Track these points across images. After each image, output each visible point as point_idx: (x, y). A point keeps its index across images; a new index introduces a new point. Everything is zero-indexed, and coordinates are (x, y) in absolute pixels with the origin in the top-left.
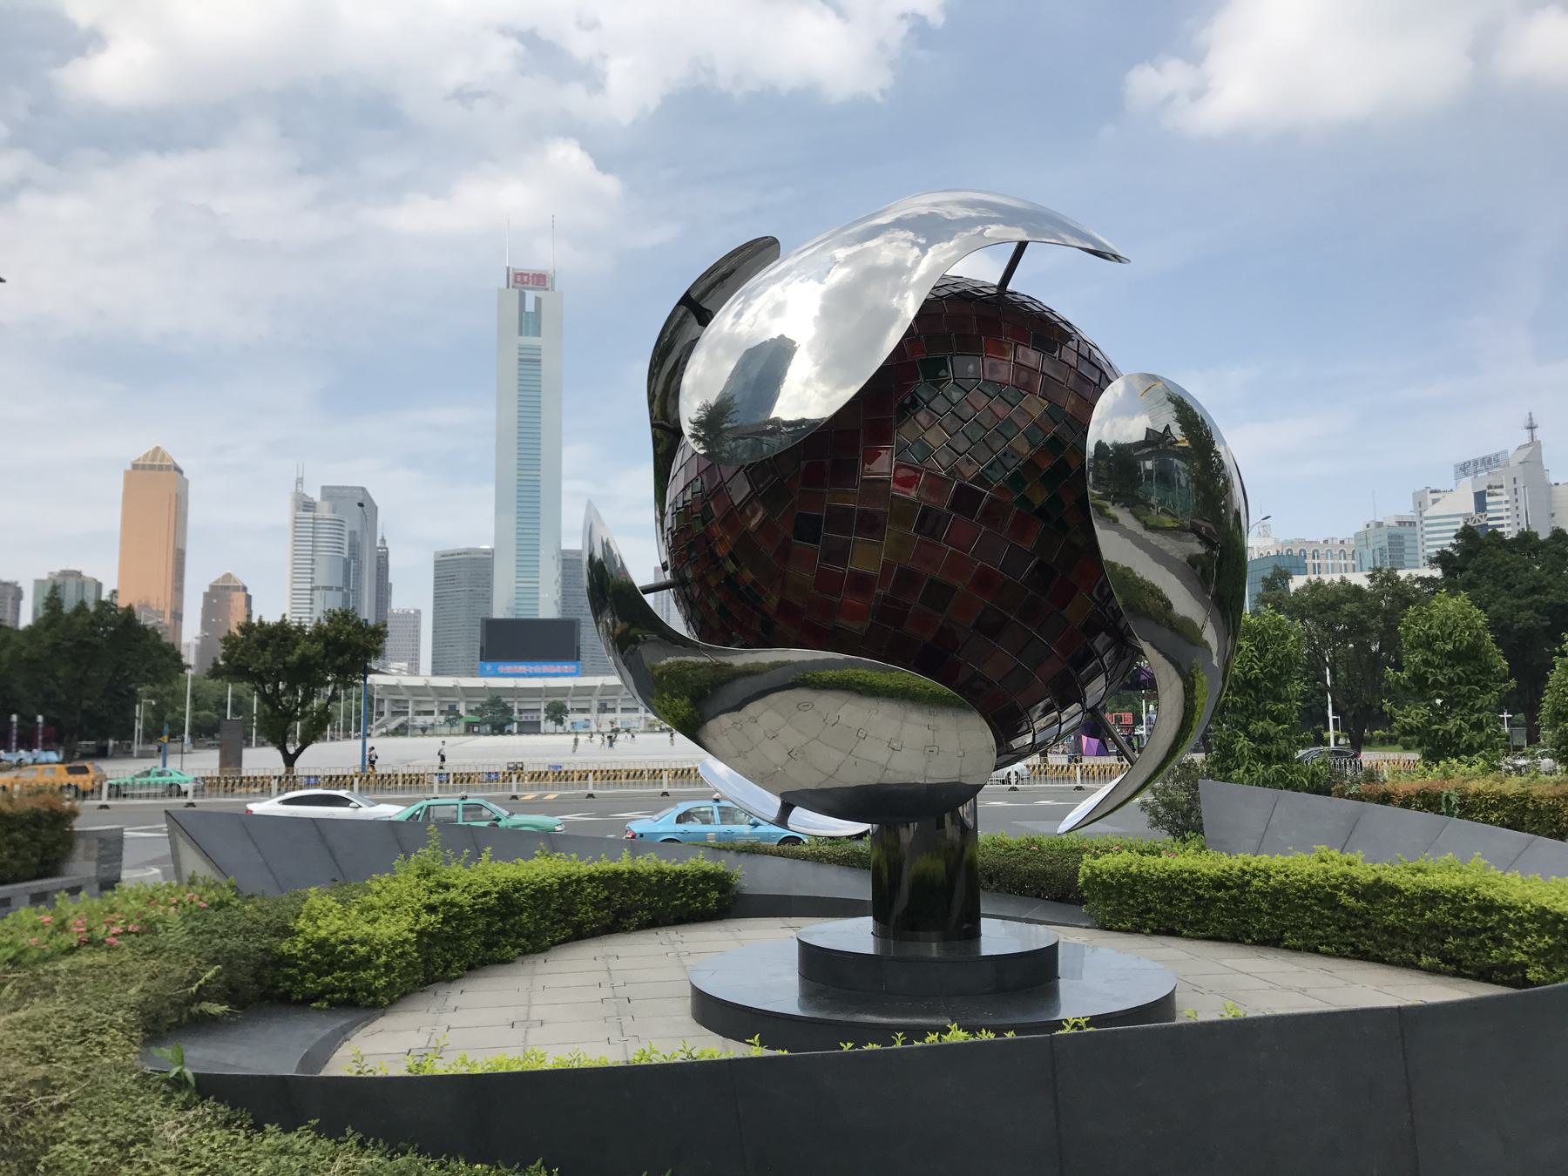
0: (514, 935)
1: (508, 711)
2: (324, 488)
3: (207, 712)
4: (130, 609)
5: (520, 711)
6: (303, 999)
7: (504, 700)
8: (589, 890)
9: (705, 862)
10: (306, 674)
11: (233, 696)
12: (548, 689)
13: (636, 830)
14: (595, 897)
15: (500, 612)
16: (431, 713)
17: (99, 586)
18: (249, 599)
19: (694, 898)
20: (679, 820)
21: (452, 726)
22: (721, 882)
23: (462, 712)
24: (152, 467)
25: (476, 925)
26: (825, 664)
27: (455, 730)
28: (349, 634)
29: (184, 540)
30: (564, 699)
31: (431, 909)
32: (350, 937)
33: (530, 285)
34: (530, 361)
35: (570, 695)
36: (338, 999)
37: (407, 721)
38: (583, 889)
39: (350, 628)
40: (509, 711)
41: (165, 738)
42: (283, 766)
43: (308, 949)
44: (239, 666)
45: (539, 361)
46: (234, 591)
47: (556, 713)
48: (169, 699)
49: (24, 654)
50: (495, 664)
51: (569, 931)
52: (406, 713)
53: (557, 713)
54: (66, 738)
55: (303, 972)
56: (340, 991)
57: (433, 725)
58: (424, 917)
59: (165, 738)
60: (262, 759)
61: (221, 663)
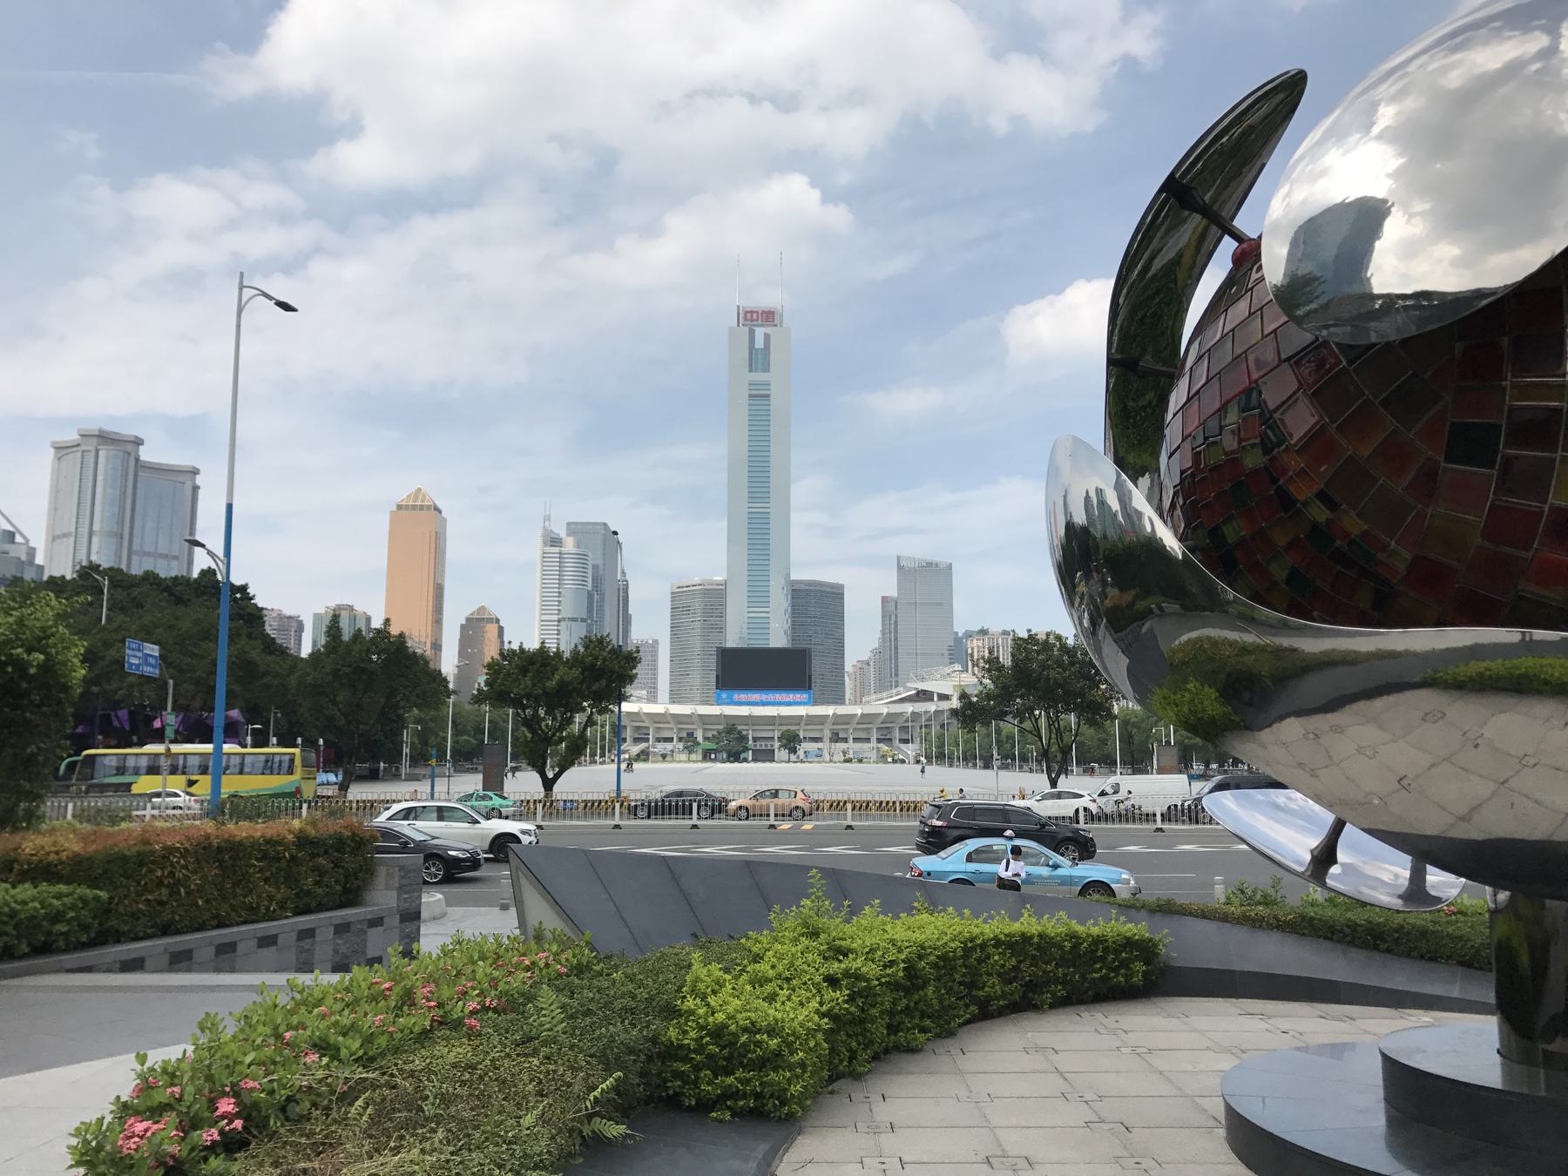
0: (917, 1014)
1: (743, 738)
2: (569, 524)
3: (466, 737)
4: (402, 635)
5: (755, 740)
6: (697, 1104)
7: (739, 728)
8: (996, 958)
9: (1129, 925)
10: (564, 699)
11: (490, 722)
12: (781, 717)
13: (923, 868)
14: (1003, 966)
15: (731, 643)
16: (670, 740)
17: (368, 619)
18: (501, 630)
19: (1116, 970)
20: (969, 858)
21: (690, 753)
22: (1144, 949)
23: (700, 739)
24: (414, 507)
25: (882, 1004)
26: (1475, 651)
27: (693, 757)
28: (604, 660)
29: (443, 575)
30: (797, 727)
31: (832, 981)
32: (753, 1023)
33: (760, 322)
34: (760, 397)
35: (802, 724)
36: (742, 1107)
37: (648, 748)
38: (988, 957)
39: (605, 654)
40: (744, 738)
41: (433, 762)
42: (543, 790)
43: (702, 1038)
44: (502, 690)
45: (768, 396)
46: (488, 622)
47: (789, 741)
48: (432, 725)
49: (309, 680)
50: (731, 692)
51: (974, 1009)
52: (647, 740)
53: (791, 742)
54: (346, 759)
55: (697, 1068)
56: (744, 1096)
57: (672, 751)
58: (830, 994)
59: (433, 762)
60: (524, 784)
61: (485, 689)
